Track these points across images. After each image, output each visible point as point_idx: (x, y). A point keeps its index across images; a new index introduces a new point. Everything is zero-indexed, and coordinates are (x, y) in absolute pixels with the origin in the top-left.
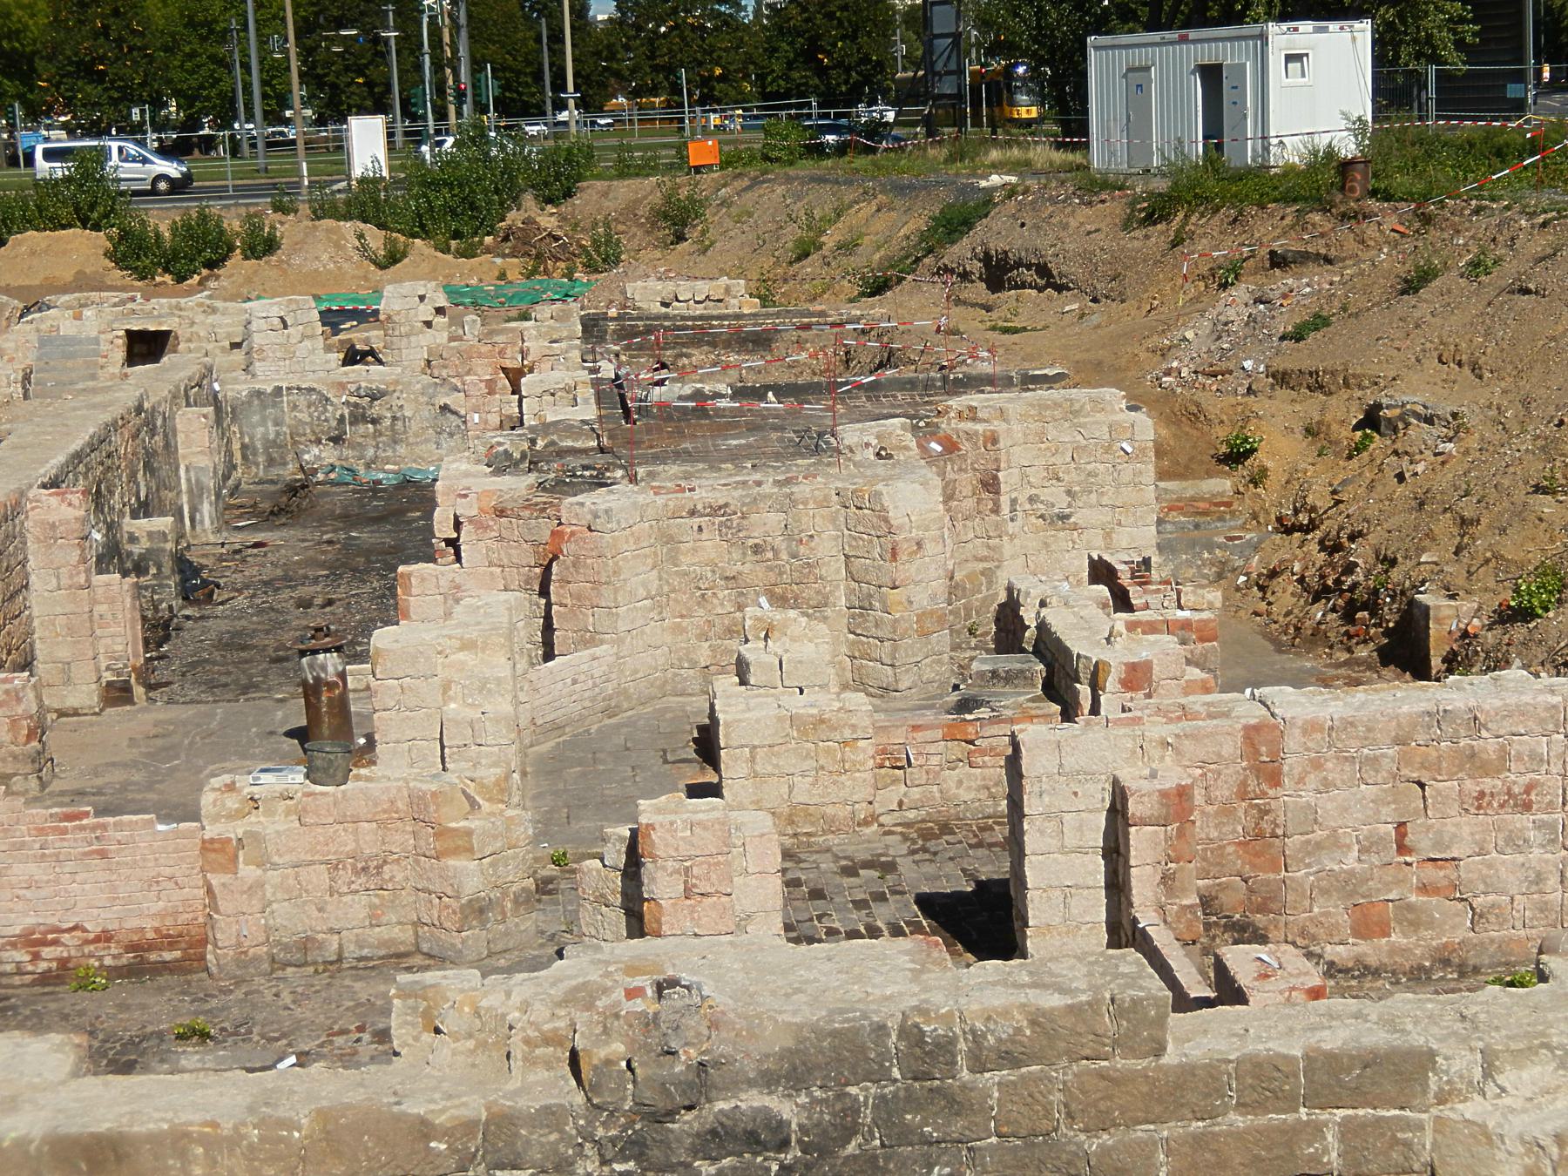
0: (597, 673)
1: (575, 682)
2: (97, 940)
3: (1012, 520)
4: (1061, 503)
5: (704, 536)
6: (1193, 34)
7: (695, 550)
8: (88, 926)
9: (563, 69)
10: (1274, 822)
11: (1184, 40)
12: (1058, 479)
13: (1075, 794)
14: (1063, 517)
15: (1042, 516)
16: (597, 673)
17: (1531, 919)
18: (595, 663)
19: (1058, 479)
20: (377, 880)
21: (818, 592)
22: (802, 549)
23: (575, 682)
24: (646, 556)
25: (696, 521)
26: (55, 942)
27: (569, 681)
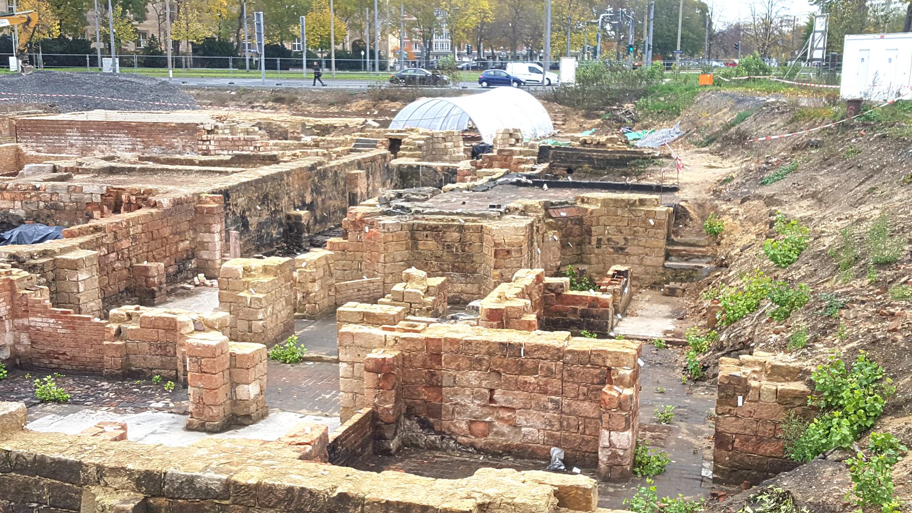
0: (371, 288)
1: (359, 290)
2: (71, 359)
3: (598, 248)
4: (622, 243)
5: (429, 239)
6: (886, 36)
7: (424, 243)
8: (68, 354)
9: (214, 166)
10: (437, 380)
11: (882, 37)
12: (621, 233)
13: (359, 355)
14: (622, 249)
15: (613, 248)
16: (371, 288)
17: (547, 441)
18: (371, 284)
19: (621, 233)
20: (164, 352)
21: (472, 267)
22: (466, 248)
23: (359, 290)
24: (402, 244)
25: (425, 233)
26: (57, 358)
27: (356, 290)
